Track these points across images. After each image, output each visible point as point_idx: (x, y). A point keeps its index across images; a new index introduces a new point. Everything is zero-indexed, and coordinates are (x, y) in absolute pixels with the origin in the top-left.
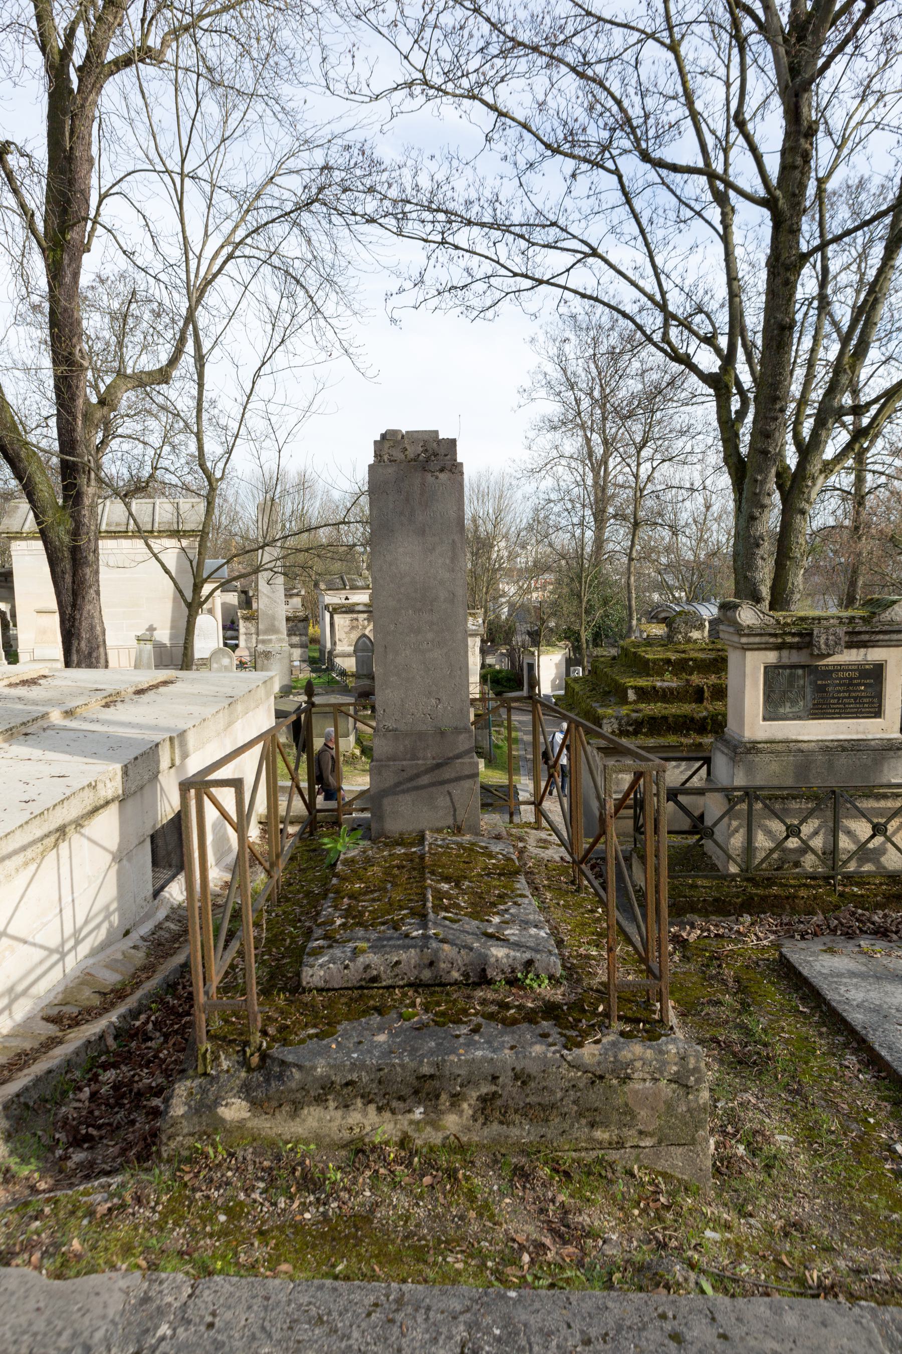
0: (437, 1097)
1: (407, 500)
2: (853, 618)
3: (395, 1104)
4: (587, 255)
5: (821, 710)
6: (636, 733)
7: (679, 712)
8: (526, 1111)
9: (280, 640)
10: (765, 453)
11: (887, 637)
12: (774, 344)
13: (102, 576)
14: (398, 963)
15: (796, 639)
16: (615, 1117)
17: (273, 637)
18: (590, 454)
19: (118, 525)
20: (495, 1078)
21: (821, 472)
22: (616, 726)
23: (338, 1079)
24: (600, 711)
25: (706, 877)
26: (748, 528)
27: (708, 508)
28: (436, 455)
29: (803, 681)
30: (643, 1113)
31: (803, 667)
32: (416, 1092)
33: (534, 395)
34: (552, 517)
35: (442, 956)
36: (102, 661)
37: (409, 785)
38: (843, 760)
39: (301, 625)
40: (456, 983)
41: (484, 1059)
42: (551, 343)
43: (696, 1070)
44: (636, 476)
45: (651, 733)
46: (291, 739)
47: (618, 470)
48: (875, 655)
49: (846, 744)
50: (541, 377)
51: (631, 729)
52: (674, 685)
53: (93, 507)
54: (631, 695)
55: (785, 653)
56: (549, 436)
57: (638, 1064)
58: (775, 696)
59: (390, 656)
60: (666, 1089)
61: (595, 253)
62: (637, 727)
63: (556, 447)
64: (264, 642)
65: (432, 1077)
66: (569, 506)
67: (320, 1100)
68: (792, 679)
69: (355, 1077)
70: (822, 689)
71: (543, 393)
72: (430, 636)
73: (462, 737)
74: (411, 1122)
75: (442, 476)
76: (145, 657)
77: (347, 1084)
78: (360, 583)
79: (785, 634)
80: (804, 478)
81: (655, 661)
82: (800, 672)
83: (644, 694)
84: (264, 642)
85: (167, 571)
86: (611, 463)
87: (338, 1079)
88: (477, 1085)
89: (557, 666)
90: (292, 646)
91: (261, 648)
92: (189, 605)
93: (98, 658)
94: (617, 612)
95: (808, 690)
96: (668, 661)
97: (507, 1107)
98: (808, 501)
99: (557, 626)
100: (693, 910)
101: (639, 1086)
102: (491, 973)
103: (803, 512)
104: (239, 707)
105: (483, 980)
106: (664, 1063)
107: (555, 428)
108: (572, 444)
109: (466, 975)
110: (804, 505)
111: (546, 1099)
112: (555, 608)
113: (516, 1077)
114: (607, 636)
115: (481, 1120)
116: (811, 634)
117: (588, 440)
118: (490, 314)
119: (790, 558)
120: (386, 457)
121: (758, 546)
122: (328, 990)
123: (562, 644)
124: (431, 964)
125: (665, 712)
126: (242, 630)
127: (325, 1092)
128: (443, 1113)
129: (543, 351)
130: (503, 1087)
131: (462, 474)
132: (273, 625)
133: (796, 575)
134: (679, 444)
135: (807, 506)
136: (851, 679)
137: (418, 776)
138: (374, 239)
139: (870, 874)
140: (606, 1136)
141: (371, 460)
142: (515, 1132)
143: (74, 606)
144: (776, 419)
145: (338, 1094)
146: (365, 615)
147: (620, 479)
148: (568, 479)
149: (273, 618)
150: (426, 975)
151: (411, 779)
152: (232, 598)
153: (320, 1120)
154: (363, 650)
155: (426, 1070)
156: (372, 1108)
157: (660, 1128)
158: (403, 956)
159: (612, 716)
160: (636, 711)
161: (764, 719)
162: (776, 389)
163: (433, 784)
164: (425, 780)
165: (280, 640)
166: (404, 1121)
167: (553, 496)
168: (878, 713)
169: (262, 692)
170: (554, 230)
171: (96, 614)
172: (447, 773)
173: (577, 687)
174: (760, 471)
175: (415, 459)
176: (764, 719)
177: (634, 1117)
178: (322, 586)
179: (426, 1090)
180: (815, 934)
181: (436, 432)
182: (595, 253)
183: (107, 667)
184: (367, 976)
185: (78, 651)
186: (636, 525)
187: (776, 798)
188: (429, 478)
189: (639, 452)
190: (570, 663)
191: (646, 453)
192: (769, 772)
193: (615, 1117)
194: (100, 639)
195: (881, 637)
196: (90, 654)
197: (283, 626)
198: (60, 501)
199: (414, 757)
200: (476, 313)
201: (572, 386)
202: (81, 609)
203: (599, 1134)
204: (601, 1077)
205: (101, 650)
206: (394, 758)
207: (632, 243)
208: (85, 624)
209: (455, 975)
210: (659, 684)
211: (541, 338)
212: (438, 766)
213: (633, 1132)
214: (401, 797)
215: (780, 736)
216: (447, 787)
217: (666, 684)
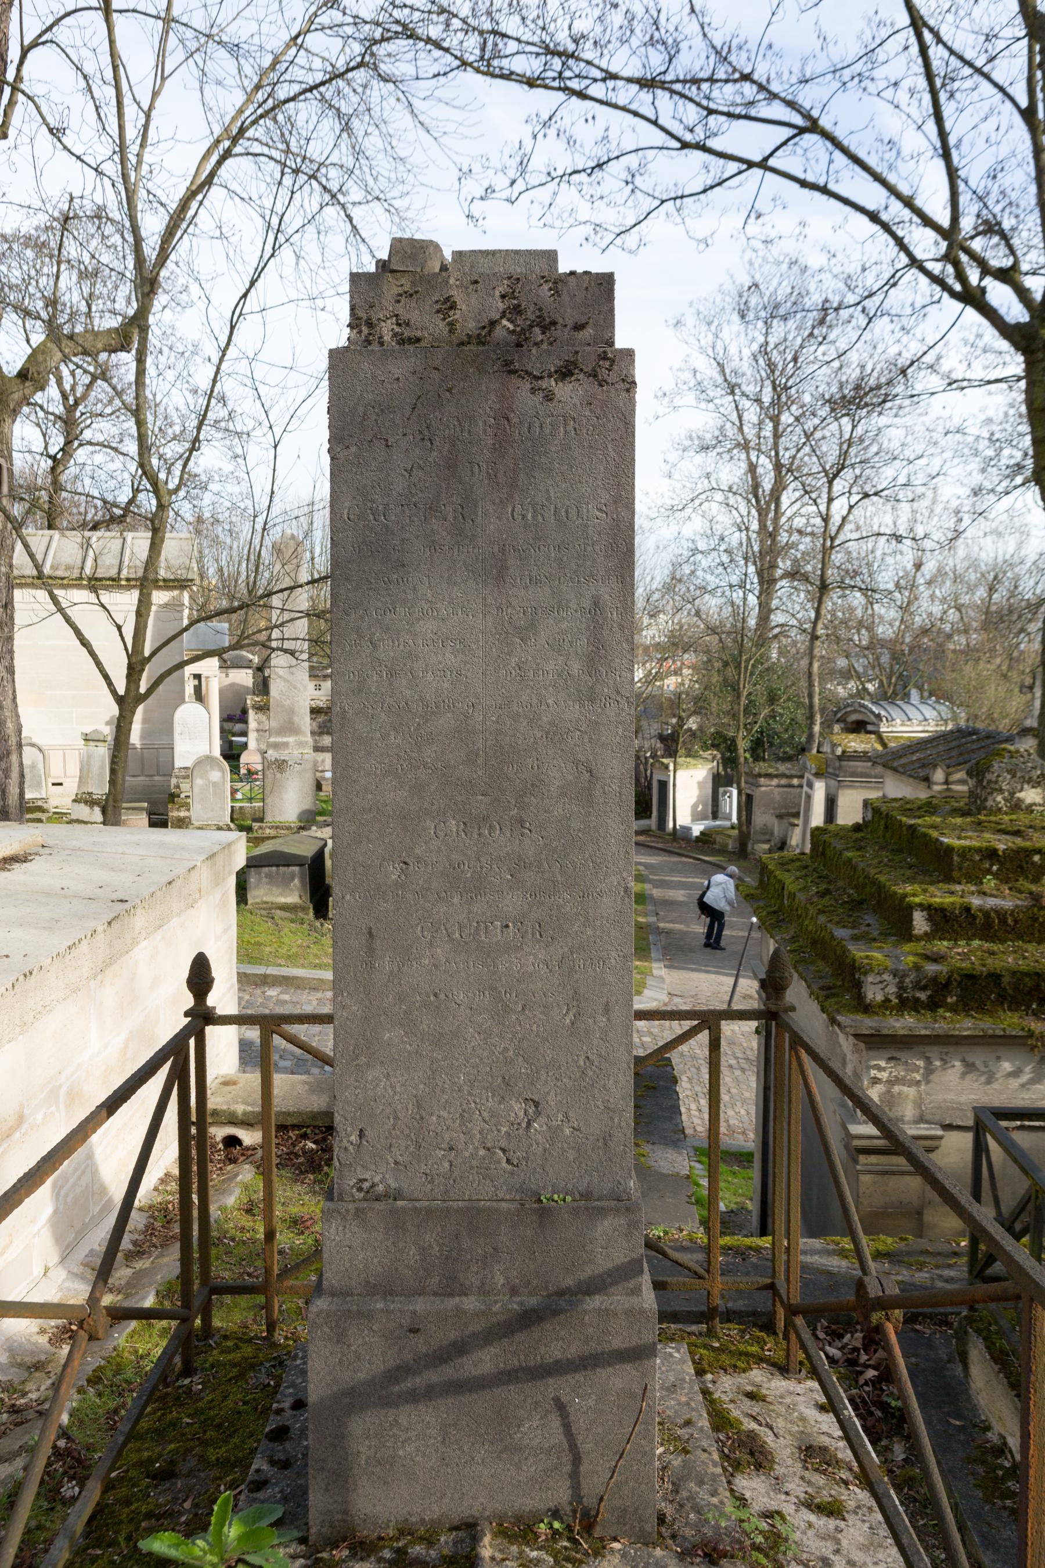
1: (451, 465)
4: (802, 131)
6: (933, 1005)
7: (1023, 965)
9: (301, 744)
17: (291, 739)
18: (756, 486)
19: (68, 568)
22: (892, 989)
24: (858, 952)
27: (918, 566)
28: (547, 325)
33: (678, 401)
34: (700, 573)
37: (433, 1377)
42: (704, 328)
44: (826, 519)
45: (964, 1007)
46: (307, 897)
47: (796, 509)
50: (688, 376)
51: (923, 996)
52: (1008, 904)
54: (920, 923)
56: (700, 458)
59: (386, 964)
61: (813, 126)
62: (935, 993)
63: (708, 476)
64: (276, 746)
66: (725, 558)
71: (690, 398)
72: (512, 903)
73: (605, 1226)
75: (564, 391)
76: (95, 765)
81: (964, 852)
83: (945, 922)
84: (276, 746)
85: (126, 649)
86: (785, 499)
89: (701, 785)
90: (317, 749)
91: (272, 754)
92: (120, 700)
94: (785, 710)
96: (991, 854)
99: (701, 728)
104: (140, 921)
107: (705, 448)
108: (732, 472)
112: (700, 705)
114: (771, 745)
117: (752, 468)
118: (631, 240)
120: (387, 329)
123: (707, 754)
125: (994, 964)
126: (252, 724)
129: (692, 340)
131: (630, 385)
132: (291, 722)
134: (889, 472)
137: (460, 1348)
138: (450, 127)
141: (339, 335)
147: (799, 522)
148: (725, 521)
149: (292, 711)
151: (442, 1356)
152: (244, 678)
159: (883, 965)
160: (935, 959)
163: (508, 1377)
164: (484, 1361)
165: (301, 744)
167: (702, 545)
169: (204, 875)
170: (749, 90)
172: (556, 1343)
173: (790, 881)
175: (483, 336)
181: (551, 256)
182: (813, 126)
186: (824, 587)
188: (525, 398)
189: (830, 483)
190: (719, 782)
191: (839, 485)
197: (306, 723)
199: (452, 1287)
200: (610, 237)
201: (732, 389)
205: (14, 758)
206: (385, 1288)
207: (888, 94)
210: (976, 901)
211: (690, 320)
212: (528, 1319)
214: (405, 1415)
216: (553, 1386)
217: (991, 902)
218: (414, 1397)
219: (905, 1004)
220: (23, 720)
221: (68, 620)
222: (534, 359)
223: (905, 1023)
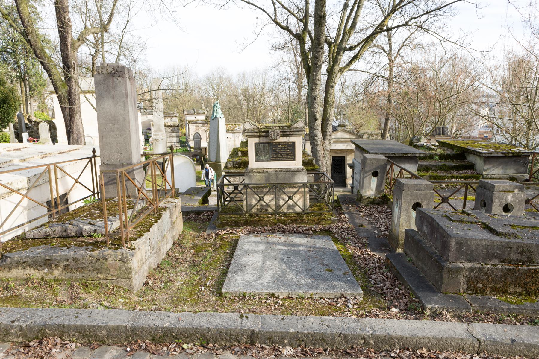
0: (51, 266)
1: (108, 87)
2: (284, 126)
3: (39, 268)
5: (275, 158)
6: (239, 167)
8: (77, 269)
9: (162, 134)
10: (316, 64)
11: (295, 133)
12: (318, 23)
13: (82, 109)
14: (55, 231)
15: (264, 134)
16: (104, 271)
17: (160, 133)
20: (68, 260)
21: (339, 72)
23: (21, 261)
25: (236, 214)
26: (311, 93)
28: (118, 71)
29: (268, 148)
30: (112, 270)
31: (268, 143)
32: (45, 264)
35: (69, 228)
36: (83, 142)
37: (112, 182)
38: (281, 175)
39: (176, 128)
40: (73, 237)
41: (64, 255)
43: (126, 257)
48: (292, 139)
49: (283, 170)
53: (77, 81)
55: (261, 138)
57: (109, 256)
58: (259, 153)
59: (104, 139)
60: (119, 263)
65: (49, 260)
67: (17, 267)
68: (264, 147)
69: (26, 260)
70: (275, 151)
72: (117, 133)
74: (44, 273)
75: (119, 78)
77: (24, 262)
78: (201, 112)
79: (260, 132)
80: (332, 74)
82: (267, 145)
85: (94, 108)
87: (21, 261)
88: (63, 262)
93: (81, 141)
95: (270, 151)
97: (72, 268)
98: (334, 83)
100: (228, 225)
101: (110, 262)
102: (84, 233)
103: (333, 87)
105: (81, 235)
106: (117, 255)
109: (76, 234)
110: (333, 84)
111: (84, 266)
113: (74, 260)
115: (64, 272)
116: (269, 132)
119: (328, 104)
120: (100, 72)
121: (315, 99)
122: (35, 239)
124: (65, 231)
127: (17, 265)
128: (53, 270)
130: (70, 262)
132: (159, 129)
133: (331, 110)
135: (334, 85)
136: (285, 147)
139: (291, 213)
140: (102, 276)
142: (75, 275)
143: (70, 121)
144: (320, 52)
145: (22, 265)
146: (202, 125)
150: (64, 234)
151: (113, 180)
153: (17, 272)
154: (197, 138)
155: (47, 258)
156: (32, 269)
157: (118, 274)
158: (57, 229)
161: (256, 161)
162: (319, 40)
165: (162, 134)
166: (42, 273)
168: (294, 159)
171: (80, 124)
174: (315, 71)
176: (256, 161)
177: (110, 271)
178: (186, 113)
179: (47, 263)
180: (262, 232)
183: (85, 145)
184: (46, 235)
185: (73, 138)
187: (259, 188)
192: (256, 179)
193: (104, 271)
194: (82, 134)
195: (293, 133)
196: (78, 140)
198: (63, 79)
202: (73, 122)
203: (100, 276)
204: (99, 260)
205: (82, 138)
208: (75, 128)
209: (73, 234)
213: (110, 275)
214: (109, 186)
215: (261, 167)
218: (110, 184)
219: (234, 167)
220: (84, 128)
221: (90, 103)
222: (116, 75)
223: (234, 170)
